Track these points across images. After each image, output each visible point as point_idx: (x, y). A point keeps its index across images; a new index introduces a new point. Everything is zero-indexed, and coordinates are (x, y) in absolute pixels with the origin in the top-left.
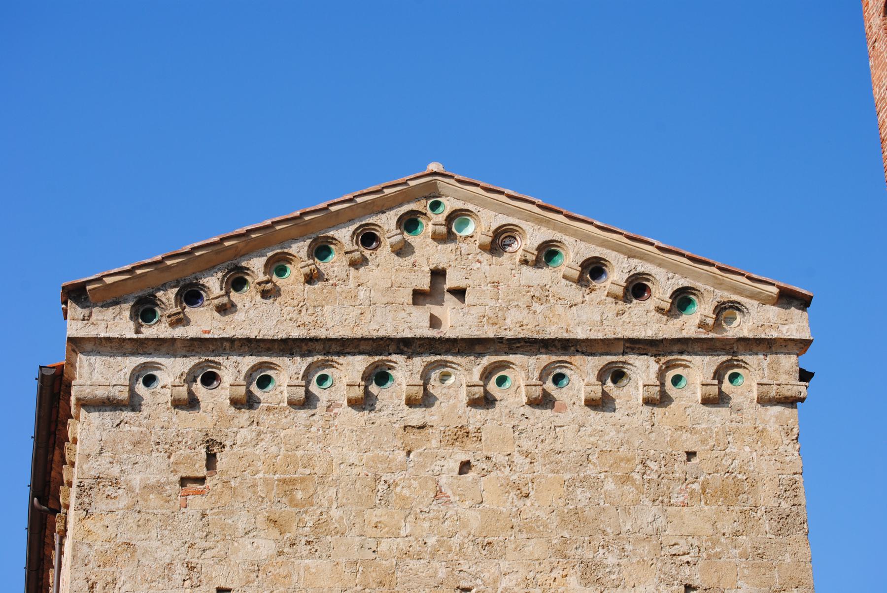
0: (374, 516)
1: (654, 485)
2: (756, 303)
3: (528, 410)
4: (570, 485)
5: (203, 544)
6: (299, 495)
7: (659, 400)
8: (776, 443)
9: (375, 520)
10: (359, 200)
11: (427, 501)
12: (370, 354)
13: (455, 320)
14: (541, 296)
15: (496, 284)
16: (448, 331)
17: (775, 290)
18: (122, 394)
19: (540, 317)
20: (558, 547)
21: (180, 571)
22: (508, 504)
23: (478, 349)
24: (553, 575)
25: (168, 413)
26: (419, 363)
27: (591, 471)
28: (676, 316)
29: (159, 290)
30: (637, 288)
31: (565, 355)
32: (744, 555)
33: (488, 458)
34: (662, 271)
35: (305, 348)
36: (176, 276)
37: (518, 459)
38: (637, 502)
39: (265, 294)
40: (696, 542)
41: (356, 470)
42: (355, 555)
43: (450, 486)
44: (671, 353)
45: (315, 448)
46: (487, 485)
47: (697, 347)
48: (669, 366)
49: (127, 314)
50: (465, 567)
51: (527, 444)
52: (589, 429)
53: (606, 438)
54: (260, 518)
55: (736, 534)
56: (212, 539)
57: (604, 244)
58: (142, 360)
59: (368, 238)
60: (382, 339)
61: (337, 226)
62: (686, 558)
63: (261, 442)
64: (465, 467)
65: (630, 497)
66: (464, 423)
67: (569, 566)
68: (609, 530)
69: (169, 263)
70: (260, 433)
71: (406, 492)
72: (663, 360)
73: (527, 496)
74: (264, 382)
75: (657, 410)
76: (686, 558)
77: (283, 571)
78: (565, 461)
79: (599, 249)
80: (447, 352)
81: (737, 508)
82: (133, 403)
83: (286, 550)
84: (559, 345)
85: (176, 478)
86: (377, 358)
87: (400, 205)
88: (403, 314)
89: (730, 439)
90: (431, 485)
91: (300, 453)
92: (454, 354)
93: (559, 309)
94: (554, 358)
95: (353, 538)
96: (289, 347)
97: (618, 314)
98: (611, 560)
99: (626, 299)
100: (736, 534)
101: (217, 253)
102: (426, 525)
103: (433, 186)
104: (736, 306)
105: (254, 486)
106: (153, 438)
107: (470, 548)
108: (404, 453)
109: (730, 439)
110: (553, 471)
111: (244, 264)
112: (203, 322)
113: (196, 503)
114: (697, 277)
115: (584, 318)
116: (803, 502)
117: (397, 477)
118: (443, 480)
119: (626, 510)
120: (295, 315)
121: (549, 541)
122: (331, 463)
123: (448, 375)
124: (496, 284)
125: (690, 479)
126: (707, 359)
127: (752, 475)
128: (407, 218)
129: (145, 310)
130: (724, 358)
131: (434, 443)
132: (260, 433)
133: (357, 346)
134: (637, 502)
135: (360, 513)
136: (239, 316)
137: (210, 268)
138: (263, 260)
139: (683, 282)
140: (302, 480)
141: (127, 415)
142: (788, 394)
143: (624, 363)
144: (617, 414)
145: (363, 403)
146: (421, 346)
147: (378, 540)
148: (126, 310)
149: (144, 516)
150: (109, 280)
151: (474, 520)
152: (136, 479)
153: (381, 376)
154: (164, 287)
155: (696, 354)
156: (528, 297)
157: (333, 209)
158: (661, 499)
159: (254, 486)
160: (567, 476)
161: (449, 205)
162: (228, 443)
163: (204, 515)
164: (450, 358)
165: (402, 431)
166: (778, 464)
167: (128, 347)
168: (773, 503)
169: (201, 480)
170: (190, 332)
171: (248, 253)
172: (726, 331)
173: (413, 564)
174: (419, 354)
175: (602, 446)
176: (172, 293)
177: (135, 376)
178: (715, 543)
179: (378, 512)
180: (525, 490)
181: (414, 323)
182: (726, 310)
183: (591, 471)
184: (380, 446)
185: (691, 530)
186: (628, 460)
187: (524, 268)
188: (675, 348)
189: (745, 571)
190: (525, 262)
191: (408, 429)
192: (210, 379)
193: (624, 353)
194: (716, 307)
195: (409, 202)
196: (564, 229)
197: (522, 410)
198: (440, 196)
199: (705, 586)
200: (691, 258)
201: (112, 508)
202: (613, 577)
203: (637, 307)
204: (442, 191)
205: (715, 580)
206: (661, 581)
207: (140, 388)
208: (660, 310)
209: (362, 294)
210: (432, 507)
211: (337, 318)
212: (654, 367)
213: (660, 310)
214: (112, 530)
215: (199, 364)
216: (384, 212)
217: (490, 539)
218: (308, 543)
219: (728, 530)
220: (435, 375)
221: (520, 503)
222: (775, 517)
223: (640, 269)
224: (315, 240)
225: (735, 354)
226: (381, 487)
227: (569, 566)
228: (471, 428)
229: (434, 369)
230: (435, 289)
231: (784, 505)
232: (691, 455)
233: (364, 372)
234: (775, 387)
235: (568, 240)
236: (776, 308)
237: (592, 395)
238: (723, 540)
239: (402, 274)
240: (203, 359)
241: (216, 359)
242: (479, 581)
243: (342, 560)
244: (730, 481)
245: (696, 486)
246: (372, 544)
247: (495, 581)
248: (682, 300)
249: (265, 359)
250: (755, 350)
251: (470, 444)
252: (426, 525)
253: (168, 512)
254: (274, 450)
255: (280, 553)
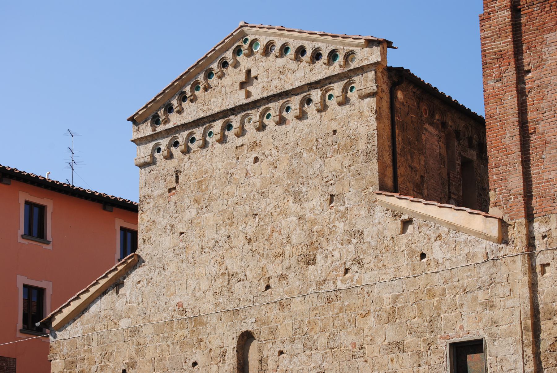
0: (227, 189)
1: (320, 150)
2: (359, 48)
3: (277, 127)
4: (290, 158)
5: (175, 215)
6: (204, 187)
7: (323, 108)
8: (367, 117)
9: (227, 191)
10: (217, 49)
11: (243, 178)
12: (223, 118)
13: (257, 91)
14: (283, 71)
15: (267, 71)
16: (255, 96)
17: (362, 41)
18: (148, 159)
19: (283, 81)
20: (286, 188)
21: (169, 228)
22: (270, 173)
23: (258, 104)
24: (285, 201)
25: (164, 163)
26: (239, 116)
27: (299, 149)
28: (332, 64)
29: (158, 110)
30: (317, 55)
31: (288, 98)
32: (353, 176)
33: (263, 153)
34: (324, 44)
35: (174, 131)
36: (163, 103)
37: (274, 151)
38: (314, 160)
39: (192, 101)
40: (335, 174)
41: (221, 171)
42: (221, 208)
43: (251, 169)
44: (326, 85)
45: (208, 165)
46: (263, 165)
47: (335, 79)
48: (327, 91)
49: (149, 124)
50: (255, 205)
51: (276, 143)
52: (298, 130)
53: (304, 132)
54: (192, 200)
55: (350, 166)
56: (178, 212)
57: (302, 39)
58: (154, 143)
59: (224, 64)
60: (224, 111)
61: (212, 63)
62: (330, 182)
63: (192, 165)
64: (256, 160)
65: (312, 158)
66: (255, 139)
67: (289, 196)
68: (304, 176)
69: (158, 99)
70: (191, 163)
71: (237, 177)
72: (324, 88)
73: (276, 167)
74: (288, 109)
75: (323, 114)
76: (330, 182)
77: (199, 221)
78: (289, 147)
79: (301, 41)
80: (248, 109)
81: (351, 153)
82: (153, 162)
83: (200, 212)
84: (284, 94)
85: (167, 190)
86: (225, 119)
87: (233, 45)
88: (236, 95)
89: (349, 120)
90: (245, 171)
91: (204, 168)
92: (251, 110)
93: (289, 75)
94: (285, 100)
95: (220, 202)
96: (197, 123)
97: (311, 71)
98: (304, 189)
99: (313, 63)
100: (350, 166)
101: (173, 89)
102: (243, 189)
103: (243, 32)
104: (352, 52)
105: (190, 186)
106: (160, 175)
107: (257, 196)
108: (236, 159)
109: (349, 120)
110: (285, 154)
111: (184, 90)
112: (175, 120)
113: (173, 198)
114: (336, 43)
115: (298, 77)
116: (376, 144)
117: (234, 170)
118: (248, 168)
119: (310, 165)
120: (202, 107)
121: (283, 186)
122: (213, 171)
123: (251, 119)
124: (267, 71)
125: (334, 144)
126: (340, 83)
127: (357, 136)
128: (237, 50)
129: (156, 121)
130: (346, 81)
131: (246, 152)
132: (191, 163)
133: (218, 116)
134: (314, 160)
135: (222, 189)
136: (185, 113)
137: (173, 97)
138: (190, 86)
139: (332, 48)
140: (204, 180)
141: (153, 167)
142: (369, 92)
143: (309, 95)
144: (308, 120)
145: (223, 140)
146: (238, 109)
147: (228, 200)
148: (149, 122)
149: (159, 208)
150: (140, 113)
151: (258, 182)
152: (156, 193)
153: (265, 114)
154: (160, 109)
155: (336, 82)
156: (279, 73)
157: (208, 56)
158: (324, 157)
159: (190, 186)
160: (290, 154)
161: (250, 38)
162: (182, 170)
163: (175, 203)
164: (249, 112)
165: (235, 149)
166: (367, 127)
167: (149, 139)
168: (364, 147)
169: (175, 188)
170: (170, 126)
171: (184, 86)
172: (351, 66)
173: (239, 207)
174: (239, 113)
175: (303, 137)
176: (162, 111)
177: (153, 150)
178: (342, 172)
179: (228, 187)
180: (275, 165)
181: (240, 98)
182: (349, 56)
183: (299, 149)
184: (228, 158)
185: (333, 168)
186: (312, 141)
187: (277, 59)
188: (327, 82)
189: (353, 183)
190: (277, 57)
191: (238, 148)
192: (176, 144)
193: (309, 90)
194: (345, 56)
195: (236, 42)
196: (287, 36)
197: (275, 128)
198: (247, 35)
199: (337, 193)
200: (331, 36)
201: (149, 207)
202: (305, 197)
203: (319, 64)
204: (247, 33)
205: (341, 190)
206: (322, 195)
207: (284, 114)
208: (325, 64)
209: (223, 90)
210: (246, 181)
211: (215, 104)
212: (320, 93)
213: (325, 64)
214: (149, 216)
215: (172, 139)
216: (228, 50)
217: (263, 191)
218: (207, 206)
219: (347, 165)
220: (246, 120)
221: (273, 171)
222: (365, 154)
223: (316, 47)
224: (206, 71)
225: (350, 77)
226: (229, 176)
227: (289, 196)
228: (258, 142)
229: (245, 118)
230: (249, 79)
231: (369, 147)
232: (335, 132)
233: (222, 127)
234: (364, 90)
235: (290, 41)
236: (367, 49)
237: (296, 114)
238: (345, 170)
239: (236, 76)
240: (285, 100)
241: (176, 135)
242: (260, 210)
243: (216, 212)
244: (349, 141)
245: (336, 147)
246: (225, 202)
247: (265, 209)
248: (333, 55)
249: (191, 130)
250: (358, 73)
251: (258, 149)
252: (243, 189)
253: (165, 205)
254: (195, 169)
255: (198, 213)
